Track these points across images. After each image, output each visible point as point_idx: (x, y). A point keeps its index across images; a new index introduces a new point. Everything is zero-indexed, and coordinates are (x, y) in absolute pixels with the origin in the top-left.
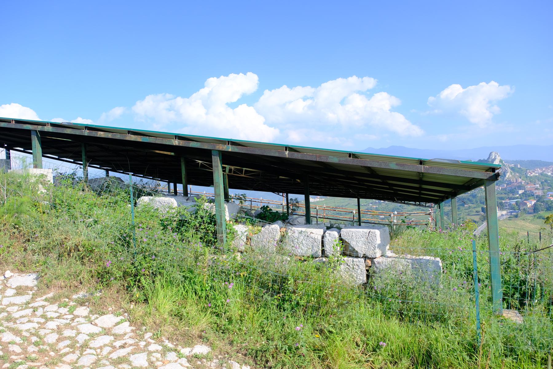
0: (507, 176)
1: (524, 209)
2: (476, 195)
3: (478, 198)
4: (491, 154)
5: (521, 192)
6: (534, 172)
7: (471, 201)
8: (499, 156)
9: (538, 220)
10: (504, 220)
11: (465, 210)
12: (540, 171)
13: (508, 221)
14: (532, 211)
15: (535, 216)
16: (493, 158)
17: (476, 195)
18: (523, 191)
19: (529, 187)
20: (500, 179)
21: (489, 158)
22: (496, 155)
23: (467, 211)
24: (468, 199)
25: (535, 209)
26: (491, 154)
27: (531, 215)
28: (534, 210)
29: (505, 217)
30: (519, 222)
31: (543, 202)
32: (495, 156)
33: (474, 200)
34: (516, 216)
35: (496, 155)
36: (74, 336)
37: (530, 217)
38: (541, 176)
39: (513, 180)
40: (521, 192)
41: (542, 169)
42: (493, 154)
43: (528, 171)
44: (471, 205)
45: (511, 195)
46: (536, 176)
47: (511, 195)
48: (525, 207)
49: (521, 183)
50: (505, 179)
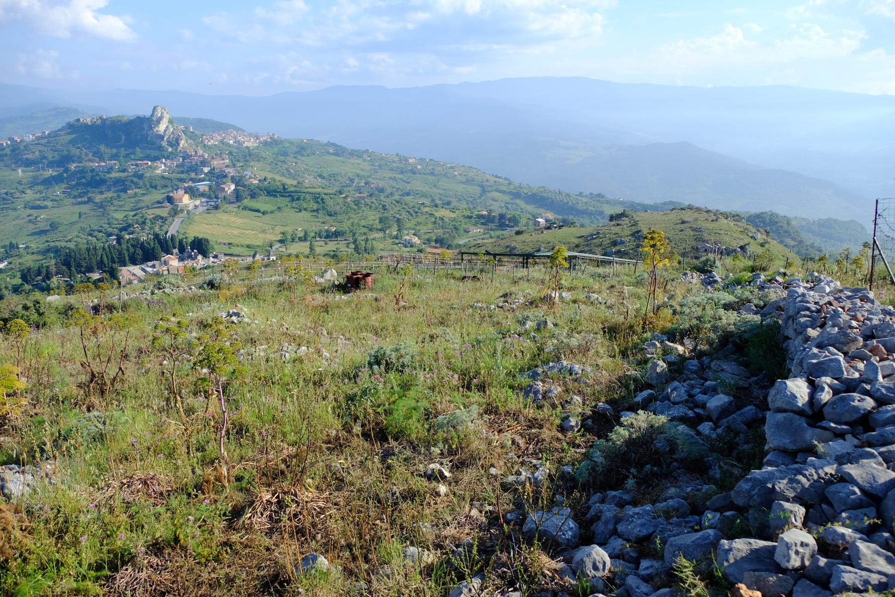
0: (181, 145)
1: (225, 198)
2: (142, 175)
3: (146, 180)
4: (155, 109)
5: (206, 170)
6: (212, 139)
7: (136, 184)
8: (167, 113)
9: (245, 212)
10: (200, 214)
11: (129, 199)
12: (219, 138)
13: (208, 215)
14: (233, 199)
15: (239, 207)
16: (159, 115)
17: (142, 175)
18: (209, 168)
19: (216, 163)
20: (856, 343)
21: (152, 115)
22: (163, 111)
23: (133, 200)
24: (132, 182)
25: (238, 196)
26: (155, 109)
27: (234, 205)
28: (237, 197)
29: (201, 209)
30: (221, 216)
31: (244, 186)
32: (162, 113)
33: (141, 183)
34: (216, 208)
35: (163, 111)
36: (618, 526)
37: (232, 208)
38: (221, 145)
39: (190, 151)
40: (206, 170)
41: (220, 135)
42: (159, 110)
43: (204, 137)
44: (137, 190)
45: (193, 175)
46: (215, 145)
47: (193, 175)
48: (224, 194)
49: (203, 156)
50: (179, 149)
